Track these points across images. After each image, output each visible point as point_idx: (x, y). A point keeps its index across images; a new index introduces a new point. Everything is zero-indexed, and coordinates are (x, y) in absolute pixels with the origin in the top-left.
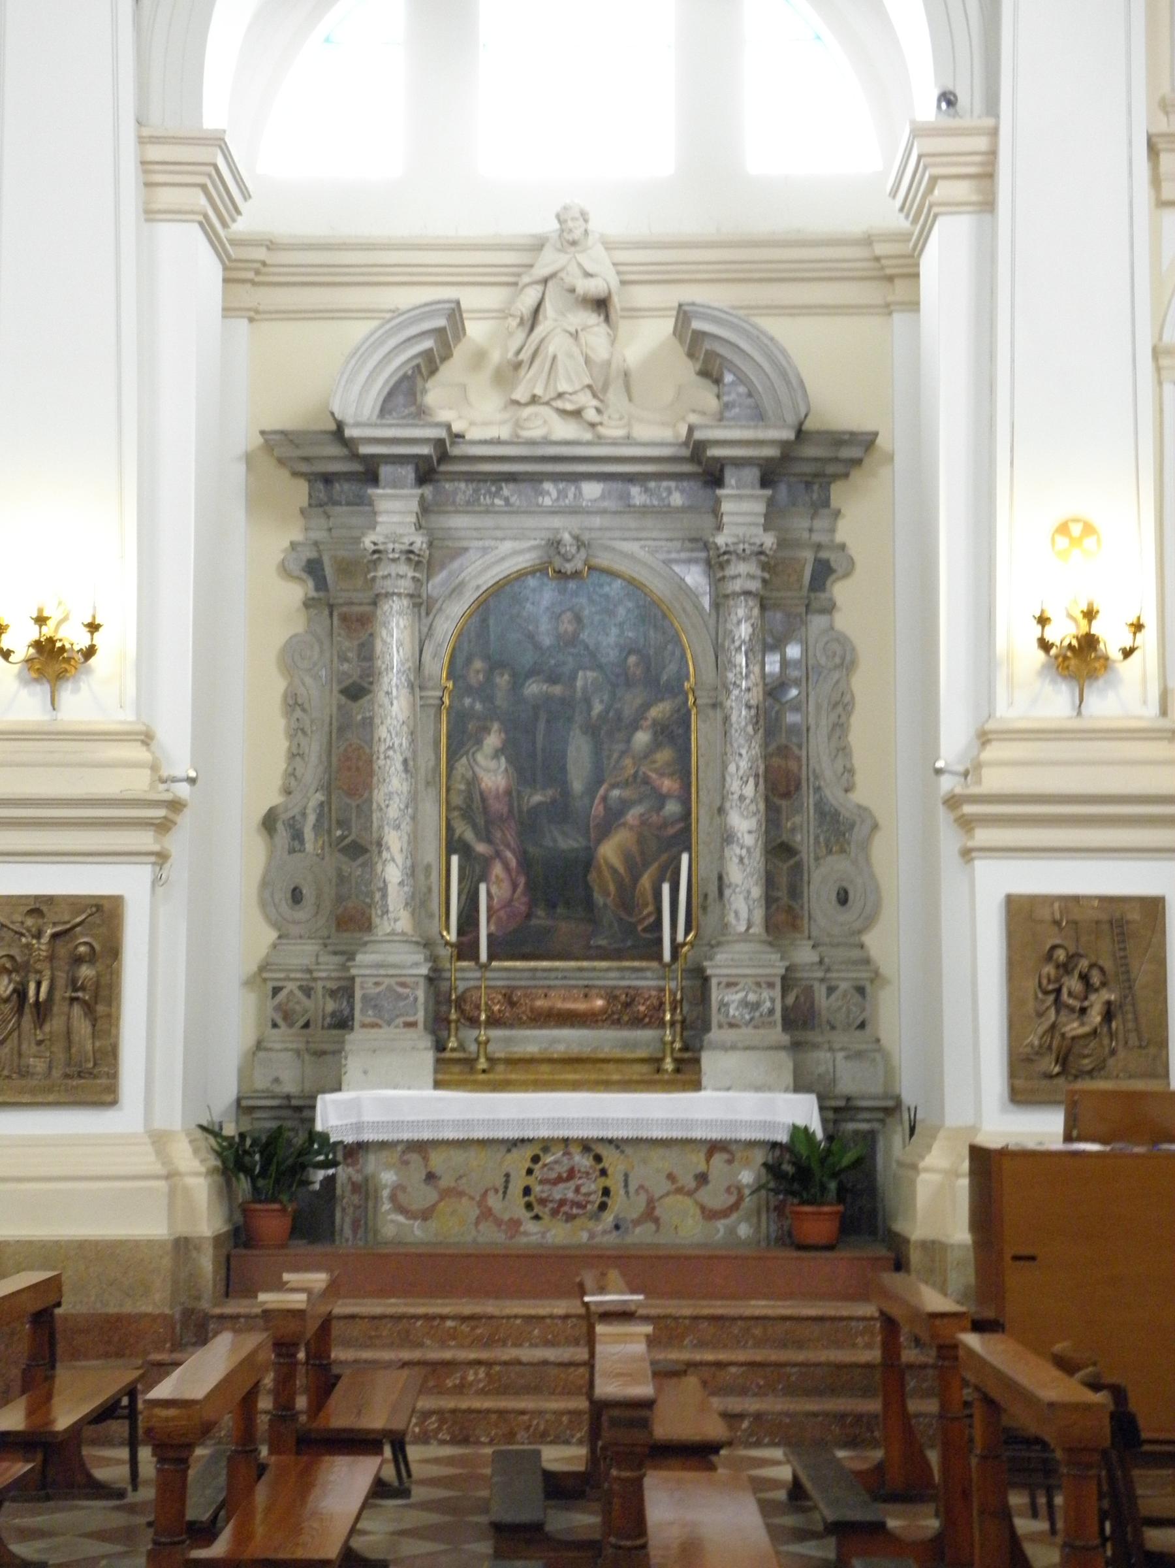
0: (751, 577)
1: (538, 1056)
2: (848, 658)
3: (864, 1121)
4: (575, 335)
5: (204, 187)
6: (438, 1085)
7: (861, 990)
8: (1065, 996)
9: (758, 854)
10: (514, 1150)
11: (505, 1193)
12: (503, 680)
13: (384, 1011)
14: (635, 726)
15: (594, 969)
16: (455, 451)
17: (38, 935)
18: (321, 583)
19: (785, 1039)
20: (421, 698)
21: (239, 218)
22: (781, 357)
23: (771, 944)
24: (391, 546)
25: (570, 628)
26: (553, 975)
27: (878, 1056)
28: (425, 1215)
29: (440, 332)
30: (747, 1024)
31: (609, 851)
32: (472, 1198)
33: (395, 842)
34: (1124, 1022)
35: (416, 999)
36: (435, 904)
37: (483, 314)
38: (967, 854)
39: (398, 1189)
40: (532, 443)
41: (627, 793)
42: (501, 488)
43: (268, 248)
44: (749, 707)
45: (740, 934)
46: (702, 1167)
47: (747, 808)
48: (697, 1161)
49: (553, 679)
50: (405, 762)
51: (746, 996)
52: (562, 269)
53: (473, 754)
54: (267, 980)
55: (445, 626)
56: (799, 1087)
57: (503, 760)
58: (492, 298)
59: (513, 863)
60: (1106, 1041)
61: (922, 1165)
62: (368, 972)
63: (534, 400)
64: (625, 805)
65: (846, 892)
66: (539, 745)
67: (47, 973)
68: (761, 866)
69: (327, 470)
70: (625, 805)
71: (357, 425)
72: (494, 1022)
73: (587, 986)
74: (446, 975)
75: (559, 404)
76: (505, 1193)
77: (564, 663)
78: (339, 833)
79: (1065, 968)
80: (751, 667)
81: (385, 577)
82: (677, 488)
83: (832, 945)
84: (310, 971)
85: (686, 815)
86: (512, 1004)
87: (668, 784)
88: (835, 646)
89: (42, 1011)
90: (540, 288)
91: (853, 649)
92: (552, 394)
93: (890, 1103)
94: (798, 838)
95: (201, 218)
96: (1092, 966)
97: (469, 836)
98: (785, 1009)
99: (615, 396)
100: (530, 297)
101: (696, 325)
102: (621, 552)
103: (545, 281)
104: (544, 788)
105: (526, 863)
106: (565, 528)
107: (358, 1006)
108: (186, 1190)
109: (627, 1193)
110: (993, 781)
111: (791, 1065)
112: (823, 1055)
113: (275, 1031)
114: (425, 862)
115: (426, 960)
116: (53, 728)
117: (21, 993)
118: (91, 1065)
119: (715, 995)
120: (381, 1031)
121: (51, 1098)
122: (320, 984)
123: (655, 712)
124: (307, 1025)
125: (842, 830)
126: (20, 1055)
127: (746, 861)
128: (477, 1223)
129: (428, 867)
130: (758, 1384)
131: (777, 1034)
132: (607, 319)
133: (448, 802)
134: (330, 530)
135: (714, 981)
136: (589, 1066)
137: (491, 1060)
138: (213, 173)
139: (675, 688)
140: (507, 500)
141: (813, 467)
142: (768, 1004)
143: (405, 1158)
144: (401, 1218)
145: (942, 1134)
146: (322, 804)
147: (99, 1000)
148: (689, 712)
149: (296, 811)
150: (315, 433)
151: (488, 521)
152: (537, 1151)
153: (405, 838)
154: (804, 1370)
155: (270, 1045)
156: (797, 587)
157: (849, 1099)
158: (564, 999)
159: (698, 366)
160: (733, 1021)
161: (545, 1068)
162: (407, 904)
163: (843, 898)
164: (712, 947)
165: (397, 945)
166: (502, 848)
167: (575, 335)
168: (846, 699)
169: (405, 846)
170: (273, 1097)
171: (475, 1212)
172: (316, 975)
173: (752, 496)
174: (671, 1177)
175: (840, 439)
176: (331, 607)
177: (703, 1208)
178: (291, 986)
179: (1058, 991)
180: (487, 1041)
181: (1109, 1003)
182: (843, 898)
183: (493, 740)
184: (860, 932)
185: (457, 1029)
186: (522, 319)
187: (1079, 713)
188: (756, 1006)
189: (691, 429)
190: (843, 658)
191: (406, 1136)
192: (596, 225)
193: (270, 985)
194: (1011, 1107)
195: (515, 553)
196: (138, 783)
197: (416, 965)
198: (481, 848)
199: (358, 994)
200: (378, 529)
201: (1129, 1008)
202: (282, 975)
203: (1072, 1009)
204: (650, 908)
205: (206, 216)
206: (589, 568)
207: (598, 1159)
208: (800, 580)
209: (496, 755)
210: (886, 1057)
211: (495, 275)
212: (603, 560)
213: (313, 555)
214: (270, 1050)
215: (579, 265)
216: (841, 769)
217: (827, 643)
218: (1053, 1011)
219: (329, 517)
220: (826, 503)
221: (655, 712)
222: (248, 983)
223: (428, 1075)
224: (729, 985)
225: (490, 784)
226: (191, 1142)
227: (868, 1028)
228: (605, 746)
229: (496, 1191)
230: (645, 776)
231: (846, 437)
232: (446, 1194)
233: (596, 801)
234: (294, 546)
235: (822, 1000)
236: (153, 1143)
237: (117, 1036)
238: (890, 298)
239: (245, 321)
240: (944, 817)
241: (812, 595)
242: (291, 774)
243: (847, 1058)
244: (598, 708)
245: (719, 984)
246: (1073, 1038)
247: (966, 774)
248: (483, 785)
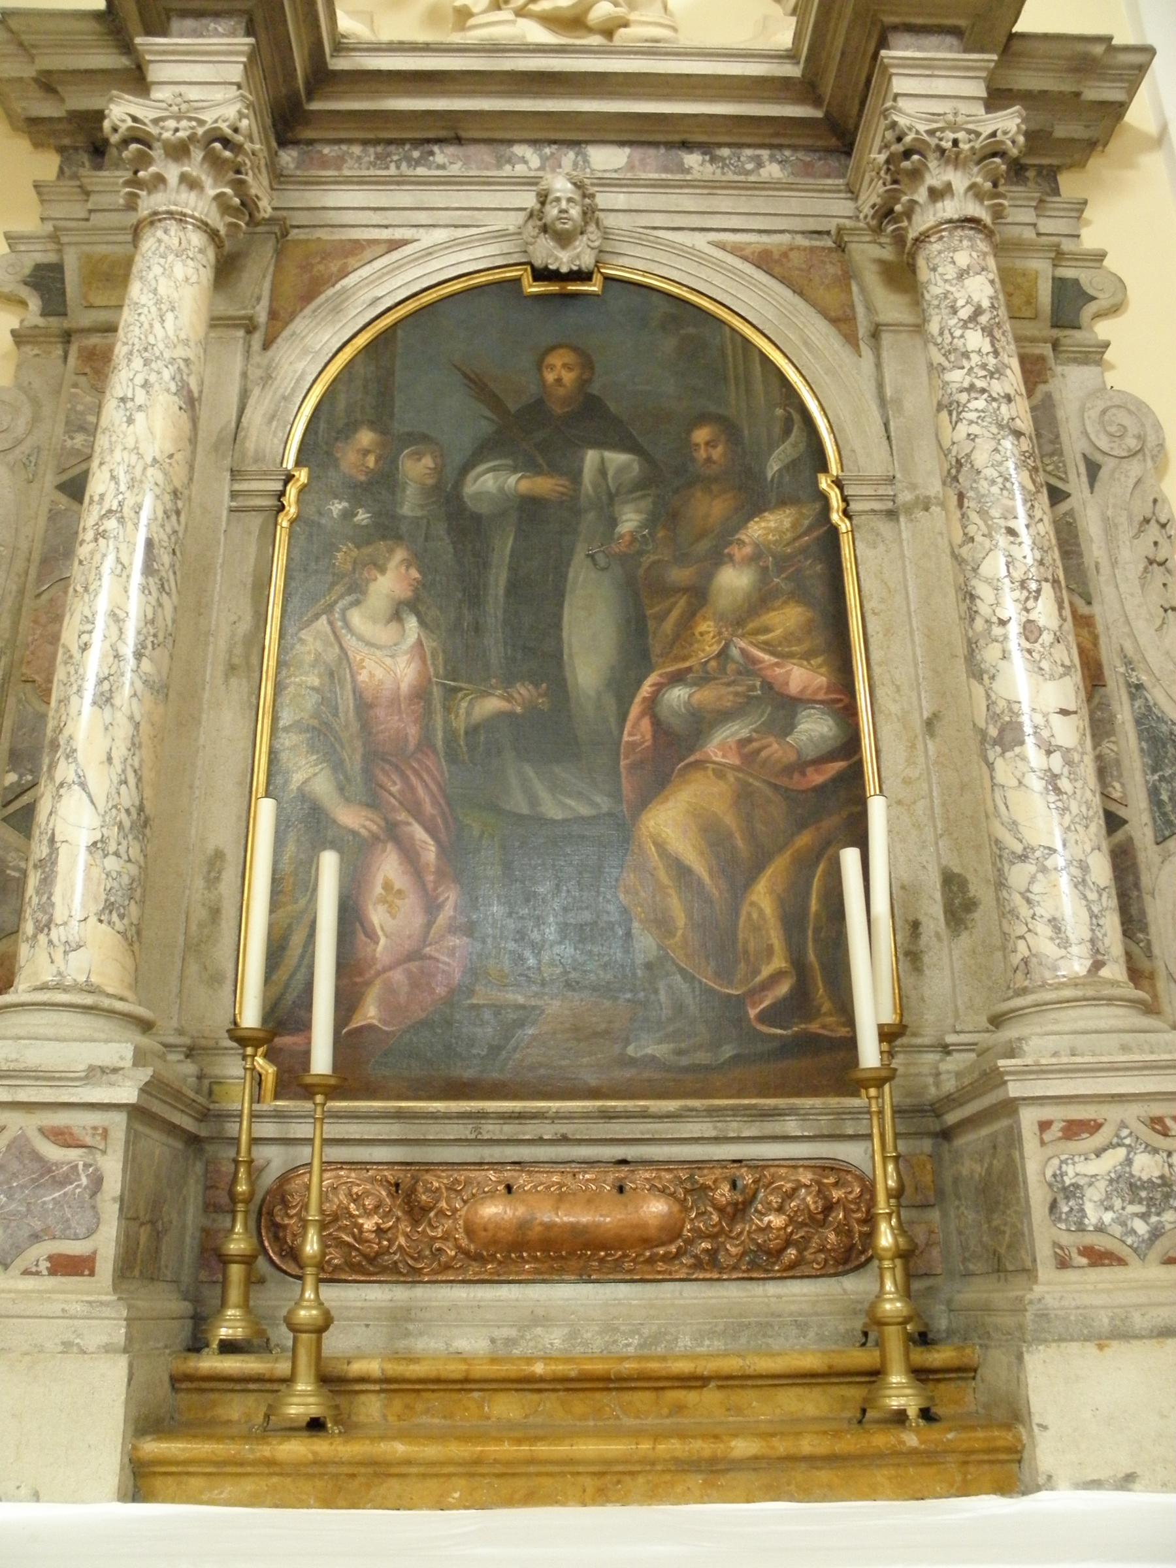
1: (482, 1369)
6: (141, 1481)
26: (530, 1130)
30: (1140, 1253)
35: (97, 1182)
41: (706, 696)
42: (432, 153)
45: (1075, 983)
51: (1129, 1162)
53: (344, 612)
55: (300, 366)
59: (430, 854)
64: (701, 724)
70: (701, 724)
72: (362, 1263)
74: (231, 1129)
82: (772, 158)
85: (850, 745)
86: (416, 1212)
91: (1158, 427)
104: (509, 680)
114: (210, 848)
115: (140, 1058)
127: (1064, 784)
136: (641, 1399)
137: (332, 1381)
153: (123, 730)
160: (1101, 1242)
161: (506, 1407)
162: (109, 907)
165: (65, 1017)
169: (120, 751)
180: (321, 1328)
185: (253, 1281)
204: (779, 962)
213: (51, 258)
217: (1104, 412)
219: (88, 194)
224: (1074, 1129)
225: (379, 673)
233: (635, 710)
248: (363, 677)
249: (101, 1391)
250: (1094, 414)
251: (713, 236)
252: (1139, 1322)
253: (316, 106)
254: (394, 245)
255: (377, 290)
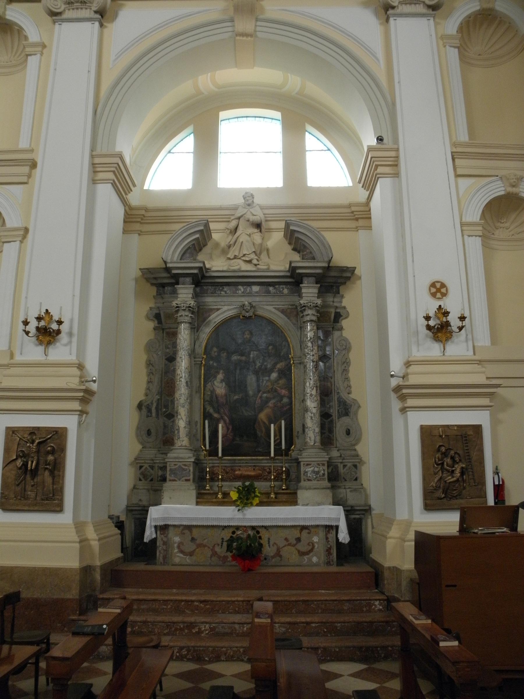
0: (314, 315)
2: (348, 347)
3: (358, 514)
4: (249, 235)
5: (114, 172)
6: (198, 503)
7: (355, 466)
8: (445, 466)
9: (318, 416)
10: (226, 529)
11: (222, 546)
12: (224, 355)
13: (179, 473)
14: (272, 371)
15: (257, 459)
16: (208, 275)
17: (33, 442)
18: (160, 322)
19: (329, 485)
20: (195, 361)
21: (131, 192)
22: (322, 238)
23: (322, 449)
24: (182, 305)
25: (248, 336)
26: (242, 462)
27: (362, 490)
28: (191, 554)
29: (201, 232)
30: (314, 480)
31: (262, 416)
32: (209, 548)
33: (183, 413)
34: (469, 475)
35: (190, 471)
36: (200, 436)
37: (218, 231)
38: (403, 410)
39: (180, 544)
40: (234, 271)
41: (269, 395)
43: (146, 211)
44: (313, 362)
45: (312, 446)
46: (298, 535)
47: (313, 398)
48: (296, 533)
49: (242, 355)
50: (187, 382)
52: (245, 214)
54: (138, 463)
56: (335, 503)
57: (224, 383)
58: (222, 226)
59: (228, 421)
60: (462, 484)
61: (388, 536)
62: (172, 460)
63: (235, 257)
64: (268, 400)
65: (349, 430)
66: (237, 378)
67: (36, 458)
68: (319, 420)
69: (161, 281)
70: (268, 400)
71: (171, 263)
73: (254, 466)
75: (244, 258)
76: (222, 546)
77: (246, 349)
78: (164, 410)
79: (445, 454)
80: (314, 347)
81: (180, 316)
82: (286, 288)
83: (344, 450)
84: (153, 460)
85: (291, 403)
87: (284, 392)
88: (343, 342)
89: (34, 473)
90: (237, 220)
91: (350, 343)
92: (241, 255)
93: (367, 508)
94: (331, 411)
95: (112, 182)
96: (455, 453)
97: (211, 411)
98: (328, 473)
99: (264, 256)
100: (233, 224)
101: (292, 228)
102: (267, 309)
103: (239, 218)
105: (232, 420)
106: (246, 301)
107: (168, 473)
108: (90, 546)
109: (269, 546)
110: (413, 380)
111: (331, 494)
112: (342, 490)
113: (141, 482)
115: (193, 456)
116: (46, 362)
117: (25, 465)
118: (51, 495)
119: (302, 469)
120: (177, 482)
121: (36, 508)
122: (157, 465)
123: (279, 366)
124: (152, 480)
125: (347, 409)
126: (25, 490)
127: (313, 418)
128: (211, 557)
129: (197, 422)
130: (324, 631)
131: (326, 483)
132: (261, 231)
133: (204, 400)
134: (163, 303)
135: (302, 463)
138: (118, 167)
139: (286, 358)
140: (226, 292)
141: (334, 279)
142: (322, 472)
143: (184, 531)
144: (181, 555)
145: (395, 523)
146: (158, 400)
147: (57, 469)
148: (291, 366)
149: (149, 402)
150: (158, 268)
151: (219, 299)
152: (234, 530)
153: (186, 411)
154: (343, 624)
155: (138, 487)
156: (330, 321)
157: (352, 507)
158: (246, 471)
159: (292, 247)
160: (309, 478)
162: (187, 435)
163: (348, 433)
164: (301, 451)
166: (223, 415)
167: (249, 235)
168: (348, 361)
169: (186, 414)
170: (139, 507)
171: (210, 553)
172: (155, 461)
173: (313, 287)
174: (286, 539)
175: (343, 270)
176: (163, 329)
177: (299, 551)
178: (146, 466)
179: (442, 464)
180: (221, 487)
181: (462, 468)
182: (348, 433)
183: (220, 376)
184: (354, 445)
186: (231, 231)
187: (444, 355)
188: (317, 473)
189: (291, 263)
190: (346, 346)
191: (185, 523)
192: (257, 200)
193: (139, 465)
194: (426, 512)
195: (228, 310)
196: (74, 382)
197: (189, 458)
198: (216, 415)
199: (168, 469)
200: (178, 299)
201: (470, 470)
202: (143, 461)
203: (448, 471)
205: (114, 181)
206: (255, 315)
207: (258, 532)
208: (330, 318)
209: (222, 381)
210: (365, 490)
211: (222, 218)
212: (260, 312)
213: (158, 312)
214: (138, 489)
215: (251, 213)
216: (346, 386)
218: (440, 472)
220: (338, 293)
221: (279, 366)
222: (131, 464)
223: (194, 500)
224: (308, 465)
225: (219, 392)
226: (94, 526)
227: (358, 480)
228: (261, 378)
229: (218, 545)
230: (276, 389)
231: (345, 268)
232: (199, 546)
233: (258, 398)
234: (151, 308)
235: (341, 470)
236: (75, 528)
237: (63, 483)
238: (357, 225)
239: (137, 235)
240: (393, 396)
241: (334, 324)
242: (148, 389)
243: (351, 491)
244: (258, 364)
245: (304, 464)
246: (450, 483)
247: (403, 378)
249: (193, 494)
250: (338, 341)
251: (274, 306)
252: (312, 487)
253: (203, 281)
254: (218, 309)
255: (216, 318)
